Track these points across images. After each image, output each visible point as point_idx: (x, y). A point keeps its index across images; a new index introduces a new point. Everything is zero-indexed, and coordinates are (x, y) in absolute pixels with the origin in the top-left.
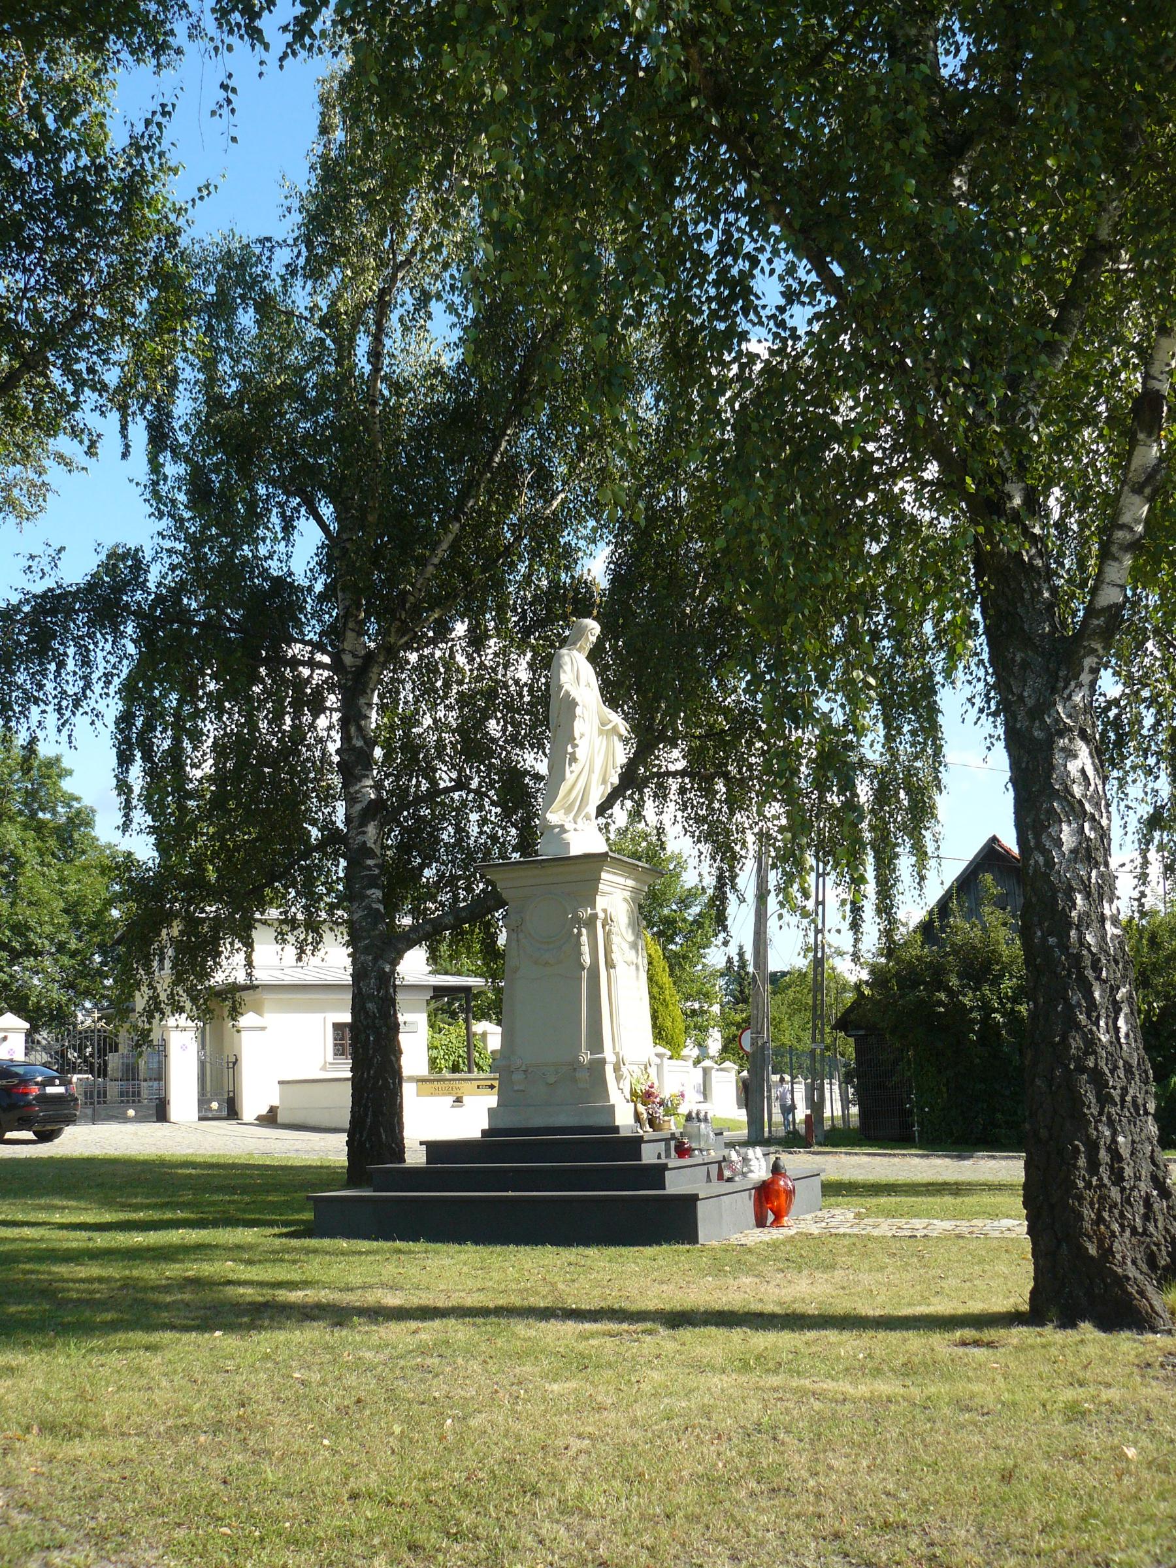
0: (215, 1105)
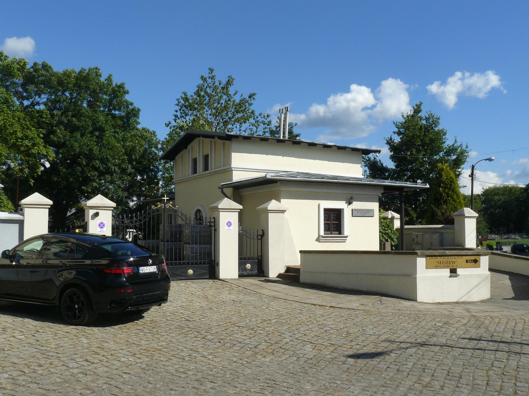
0: (248, 266)
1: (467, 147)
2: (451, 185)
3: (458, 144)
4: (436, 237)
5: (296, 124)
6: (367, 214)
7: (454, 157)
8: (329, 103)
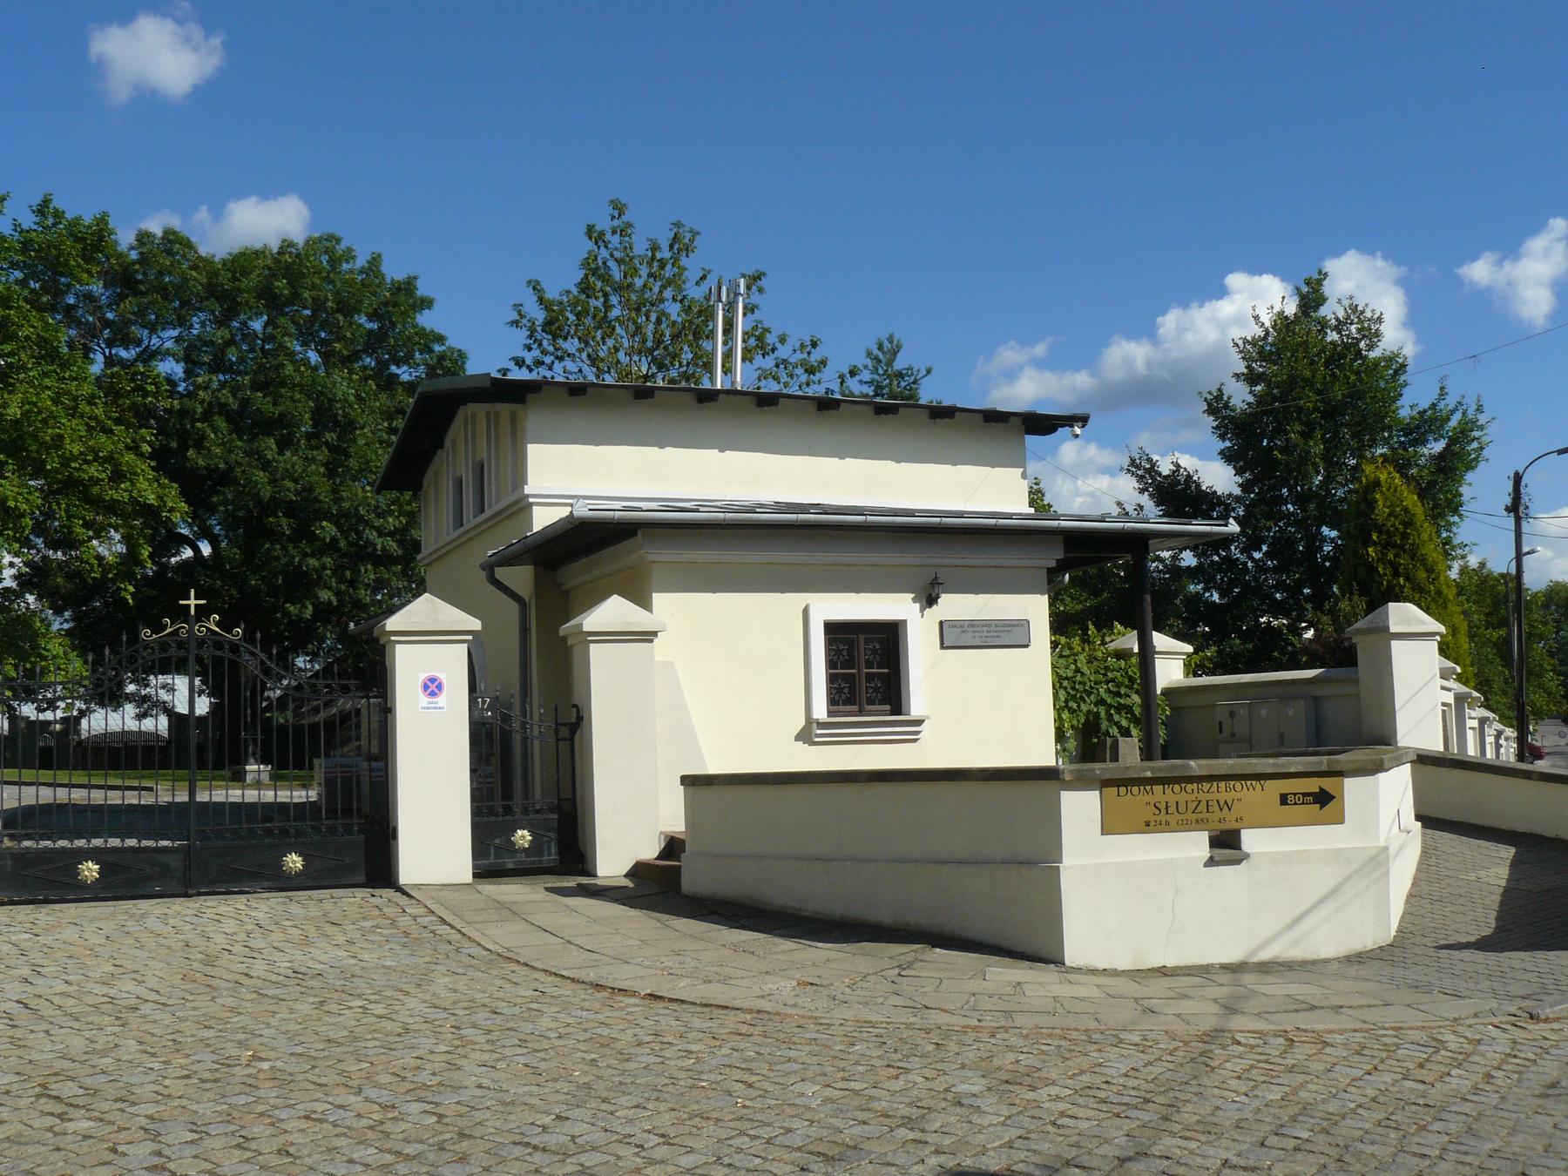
0: (523, 837)
1: (1479, 409)
2: (1405, 536)
3: (1451, 401)
4: (1296, 712)
5: (929, 371)
6: (1010, 635)
7: (1438, 447)
8: (1162, 331)
